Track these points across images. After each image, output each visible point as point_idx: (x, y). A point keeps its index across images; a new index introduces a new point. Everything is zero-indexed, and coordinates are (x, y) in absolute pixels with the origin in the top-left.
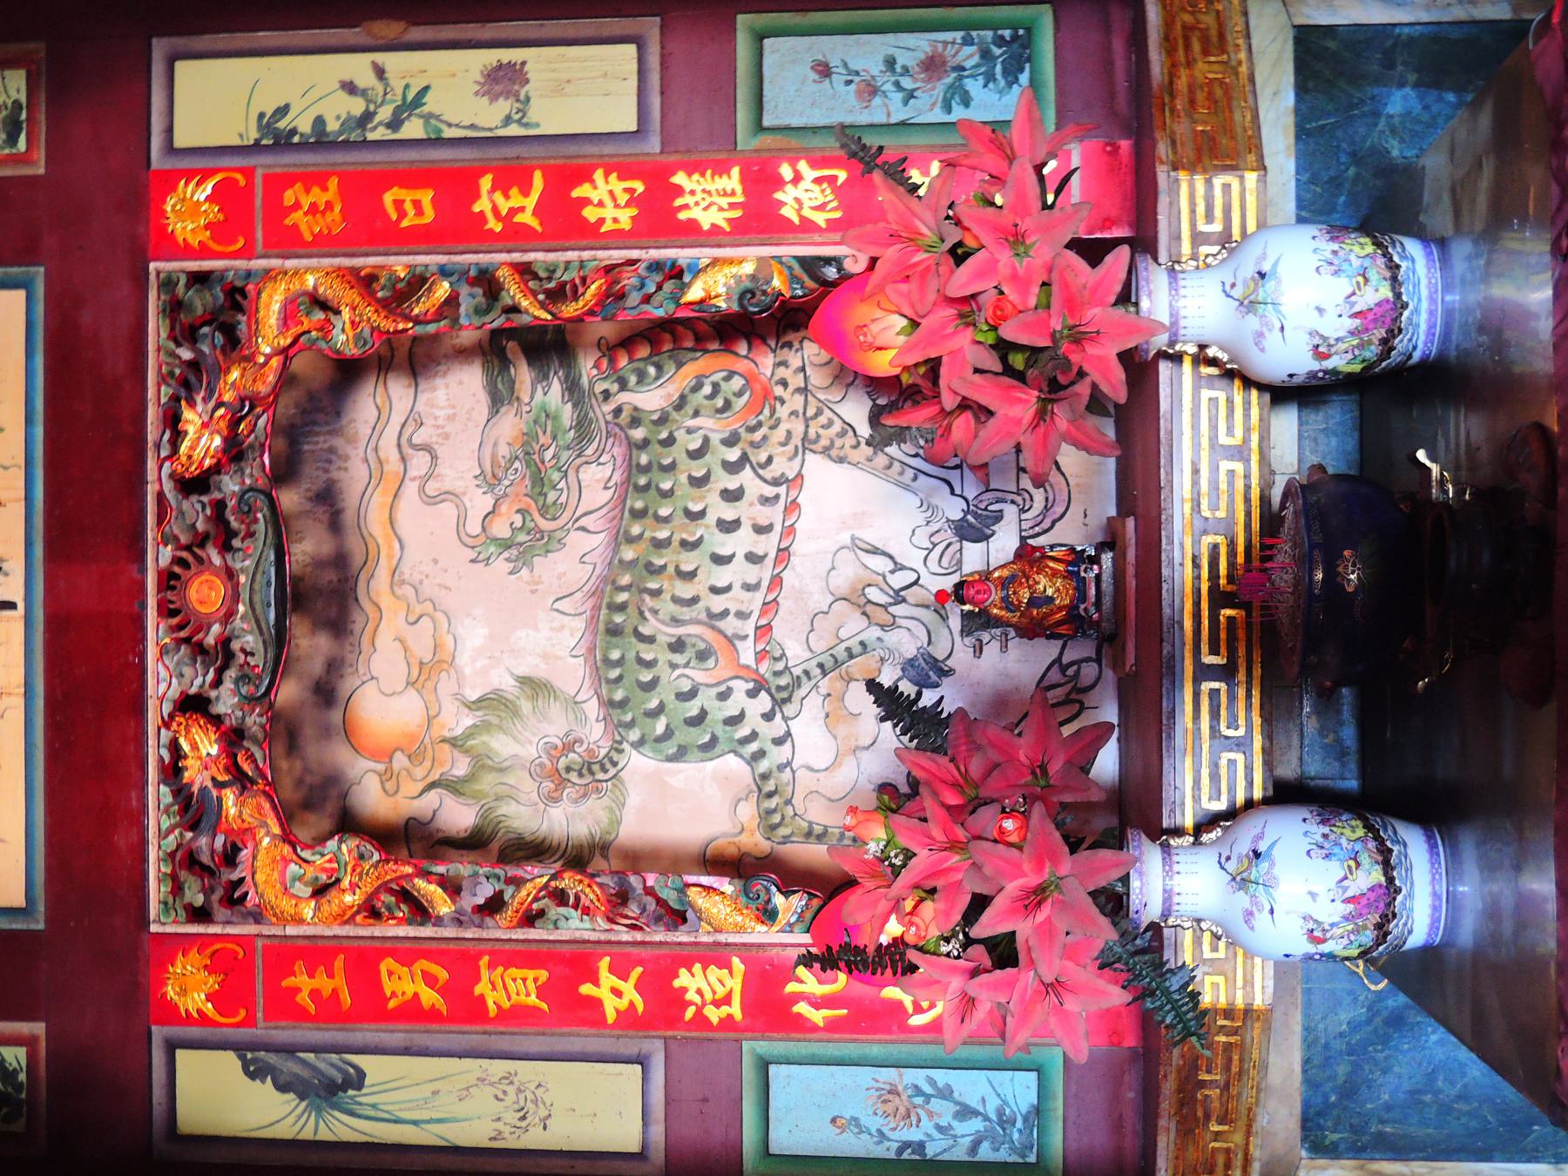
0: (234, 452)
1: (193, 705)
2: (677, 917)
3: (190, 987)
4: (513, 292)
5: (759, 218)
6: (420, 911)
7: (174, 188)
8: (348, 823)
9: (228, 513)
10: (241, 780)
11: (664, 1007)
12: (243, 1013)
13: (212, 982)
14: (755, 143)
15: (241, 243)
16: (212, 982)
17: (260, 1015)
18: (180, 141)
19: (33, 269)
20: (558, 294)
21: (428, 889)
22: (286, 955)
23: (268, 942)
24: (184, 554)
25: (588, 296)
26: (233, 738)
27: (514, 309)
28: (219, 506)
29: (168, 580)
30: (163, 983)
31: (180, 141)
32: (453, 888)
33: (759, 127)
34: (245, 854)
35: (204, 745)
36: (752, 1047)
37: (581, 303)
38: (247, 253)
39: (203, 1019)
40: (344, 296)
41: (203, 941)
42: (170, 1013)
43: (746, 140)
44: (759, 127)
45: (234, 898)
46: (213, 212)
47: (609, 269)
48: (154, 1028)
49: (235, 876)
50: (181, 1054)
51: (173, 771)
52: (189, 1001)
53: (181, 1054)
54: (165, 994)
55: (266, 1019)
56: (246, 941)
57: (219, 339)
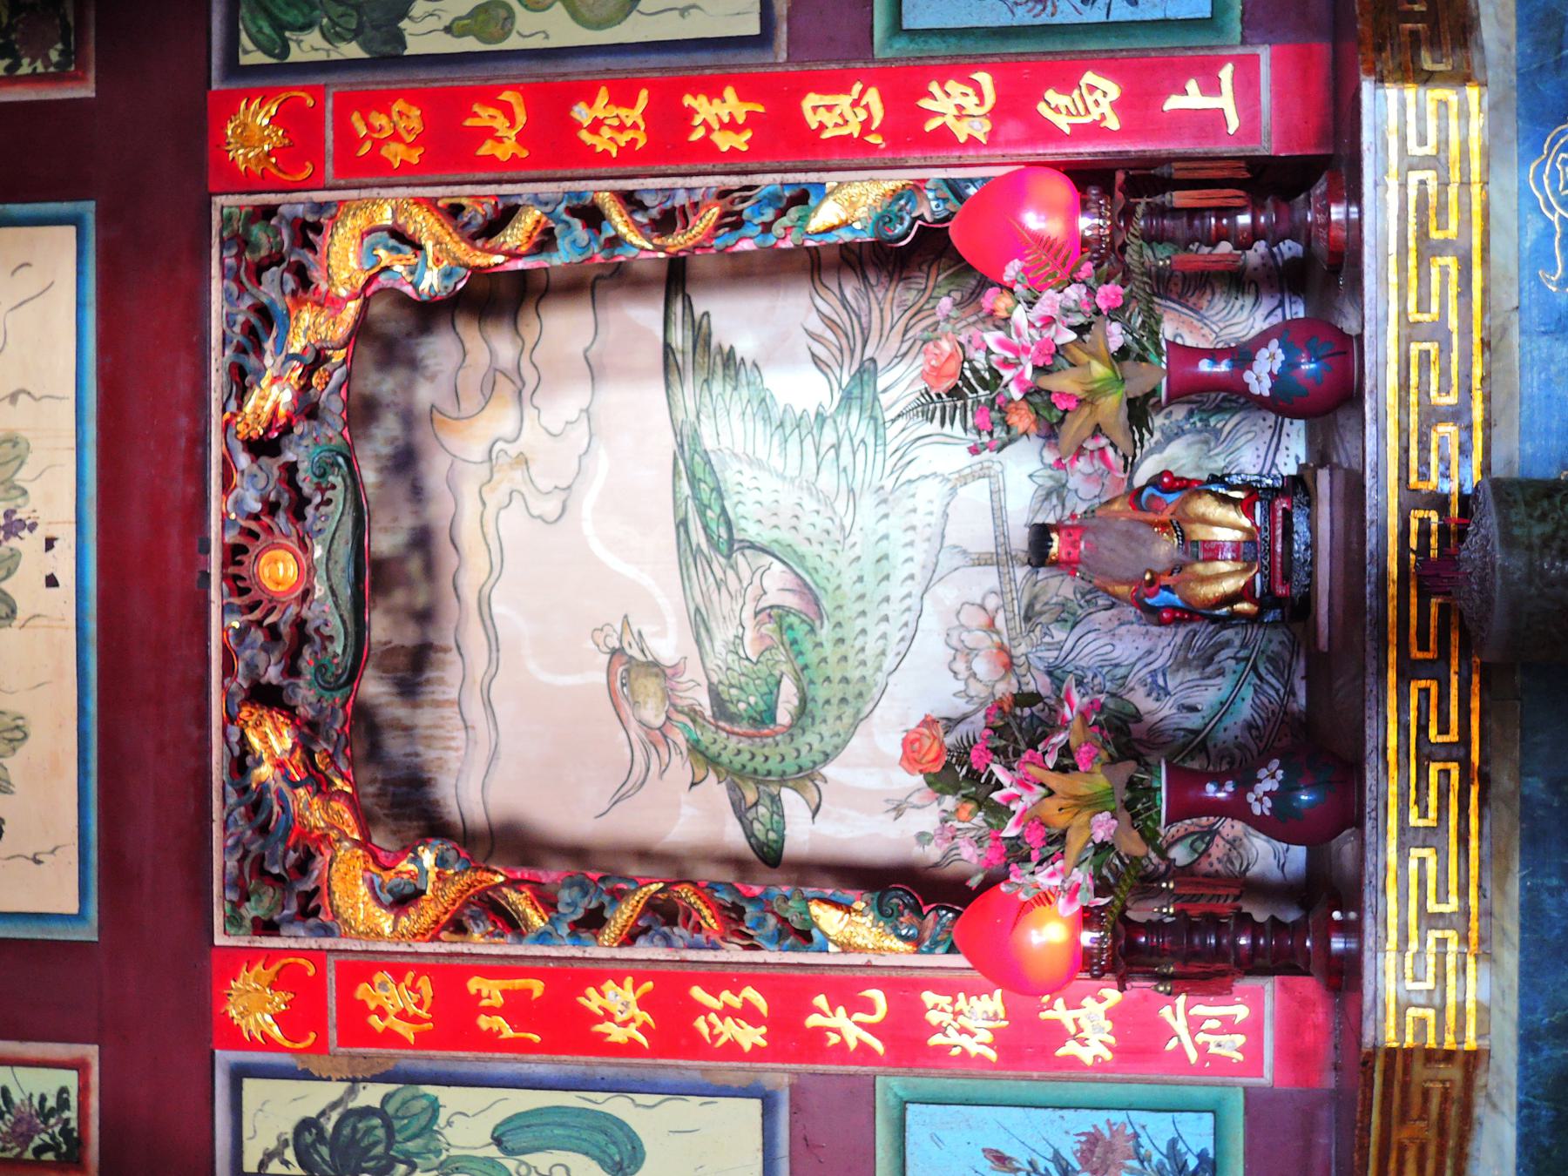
0: (308, 409)
1: (266, 697)
2: (804, 937)
3: (254, 1005)
4: (618, 221)
5: (908, 133)
6: (511, 924)
7: (235, 111)
8: (435, 826)
9: (301, 475)
10: (320, 785)
11: (791, 1037)
12: (313, 1036)
13: (280, 1001)
14: (901, 47)
15: (309, 171)
16: (280, 1001)
17: (333, 1035)
18: (70, 232)
19: (224, 87)
20: (667, 222)
21: (518, 900)
22: (358, 970)
23: (343, 957)
24: (253, 525)
25: (696, 230)
26: (308, 733)
27: (616, 241)
28: (291, 469)
29: (234, 554)
30: (225, 999)
31: (70, 232)
32: (547, 902)
33: (897, 27)
34: (320, 863)
35: (274, 741)
36: (890, 1086)
37: (690, 235)
38: (315, 183)
39: (270, 1044)
40: (423, 224)
41: (271, 955)
42: (234, 1038)
43: (883, 47)
44: (897, 27)
45: (309, 907)
46: (277, 136)
47: (724, 194)
48: (217, 1052)
49: (309, 886)
50: (249, 1084)
51: (241, 763)
52: (252, 1021)
53: (249, 1084)
54: (226, 1013)
55: (342, 1042)
56: (317, 956)
57: (291, 284)
